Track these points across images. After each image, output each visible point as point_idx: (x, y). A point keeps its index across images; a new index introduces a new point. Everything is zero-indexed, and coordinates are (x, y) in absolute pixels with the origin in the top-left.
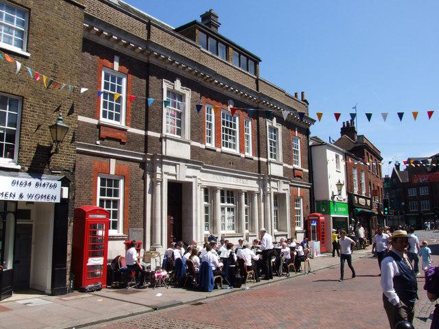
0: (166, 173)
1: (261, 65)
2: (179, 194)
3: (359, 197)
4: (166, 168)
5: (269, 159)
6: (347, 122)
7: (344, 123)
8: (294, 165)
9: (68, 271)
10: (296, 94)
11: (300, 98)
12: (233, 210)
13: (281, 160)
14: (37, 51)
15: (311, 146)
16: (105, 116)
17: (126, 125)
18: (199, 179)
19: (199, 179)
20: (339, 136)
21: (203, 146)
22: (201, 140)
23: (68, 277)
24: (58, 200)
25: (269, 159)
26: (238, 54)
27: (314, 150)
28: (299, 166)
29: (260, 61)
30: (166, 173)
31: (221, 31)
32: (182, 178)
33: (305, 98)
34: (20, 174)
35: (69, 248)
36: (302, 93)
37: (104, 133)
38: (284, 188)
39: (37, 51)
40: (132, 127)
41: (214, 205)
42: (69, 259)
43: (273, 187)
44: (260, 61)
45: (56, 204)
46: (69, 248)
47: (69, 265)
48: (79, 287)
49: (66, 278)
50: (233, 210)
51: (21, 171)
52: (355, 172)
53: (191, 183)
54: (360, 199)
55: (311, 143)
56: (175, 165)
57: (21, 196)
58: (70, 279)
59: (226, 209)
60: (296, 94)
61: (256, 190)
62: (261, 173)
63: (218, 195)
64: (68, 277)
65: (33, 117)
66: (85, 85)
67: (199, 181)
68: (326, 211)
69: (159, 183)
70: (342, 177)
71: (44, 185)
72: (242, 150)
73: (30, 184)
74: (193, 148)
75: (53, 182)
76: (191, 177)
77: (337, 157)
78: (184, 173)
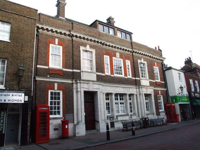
0: (83, 87)
1: (133, 35)
2: (90, 97)
3: (194, 93)
4: (82, 85)
5: (141, 78)
6: (187, 58)
7: (186, 59)
8: (156, 80)
9: (29, 133)
10: (156, 48)
11: (157, 49)
12: (123, 103)
13: (148, 78)
14: (14, 39)
15: (165, 71)
16: (115, 74)
17: (63, 68)
18: (102, 89)
19: (102, 89)
20: (184, 65)
21: (104, 75)
22: (154, 79)
23: (28, 137)
24: (23, 102)
25: (141, 78)
26: (120, 32)
27: (166, 72)
28: (159, 81)
29: (132, 34)
30: (83, 87)
31: (116, 25)
32: (91, 89)
33: (160, 49)
34: (5, 91)
35: (29, 124)
36: (159, 47)
37: (50, 72)
38: (150, 91)
39: (14, 39)
40: (65, 68)
41: (112, 101)
42: (29, 128)
43: (144, 91)
44: (132, 34)
45: (23, 103)
46: (29, 124)
47: (29, 131)
48: (34, 141)
49: (27, 137)
50: (123, 103)
51: (6, 90)
52: (191, 81)
53: (97, 92)
54: (196, 94)
55: (164, 69)
56: (88, 83)
57: (5, 101)
58: (29, 138)
59: (119, 103)
60: (156, 48)
61: (135, 93)
62: (137, 83)
63: (128, 97)
64: (28, 137)
65: (11, 66)
66: (79, 58)
67: (101, 91)
68: (175, 101)
69: (80, 92)
70: (184, 84)
71: (16, 95)
72: (126, 75)
73: (9, 95)
74: (97, 76)
75: (20, 94)
76: (96, 89)
77: (179, 74)
78: (92, 87)
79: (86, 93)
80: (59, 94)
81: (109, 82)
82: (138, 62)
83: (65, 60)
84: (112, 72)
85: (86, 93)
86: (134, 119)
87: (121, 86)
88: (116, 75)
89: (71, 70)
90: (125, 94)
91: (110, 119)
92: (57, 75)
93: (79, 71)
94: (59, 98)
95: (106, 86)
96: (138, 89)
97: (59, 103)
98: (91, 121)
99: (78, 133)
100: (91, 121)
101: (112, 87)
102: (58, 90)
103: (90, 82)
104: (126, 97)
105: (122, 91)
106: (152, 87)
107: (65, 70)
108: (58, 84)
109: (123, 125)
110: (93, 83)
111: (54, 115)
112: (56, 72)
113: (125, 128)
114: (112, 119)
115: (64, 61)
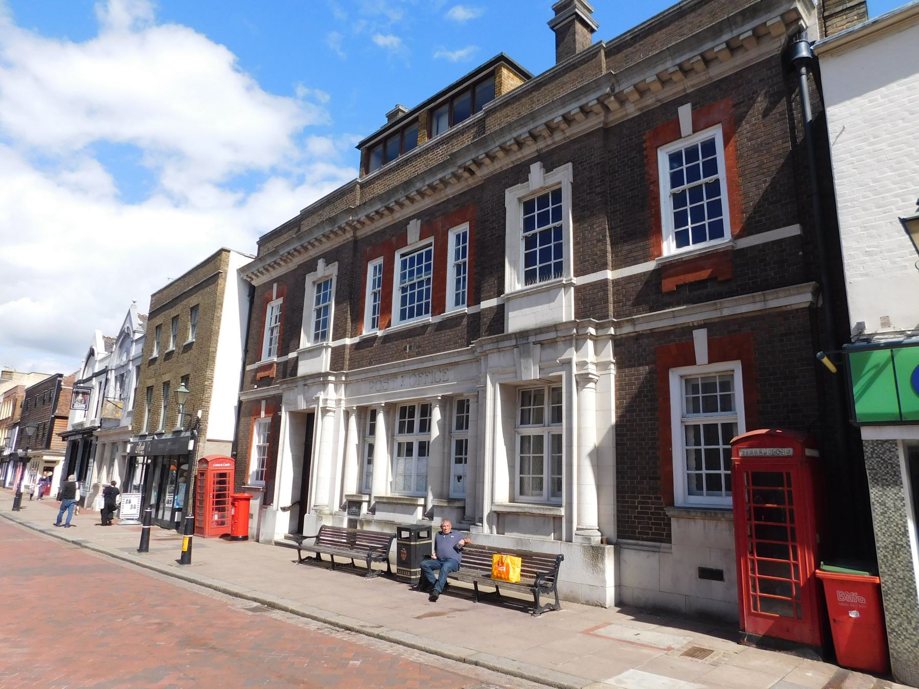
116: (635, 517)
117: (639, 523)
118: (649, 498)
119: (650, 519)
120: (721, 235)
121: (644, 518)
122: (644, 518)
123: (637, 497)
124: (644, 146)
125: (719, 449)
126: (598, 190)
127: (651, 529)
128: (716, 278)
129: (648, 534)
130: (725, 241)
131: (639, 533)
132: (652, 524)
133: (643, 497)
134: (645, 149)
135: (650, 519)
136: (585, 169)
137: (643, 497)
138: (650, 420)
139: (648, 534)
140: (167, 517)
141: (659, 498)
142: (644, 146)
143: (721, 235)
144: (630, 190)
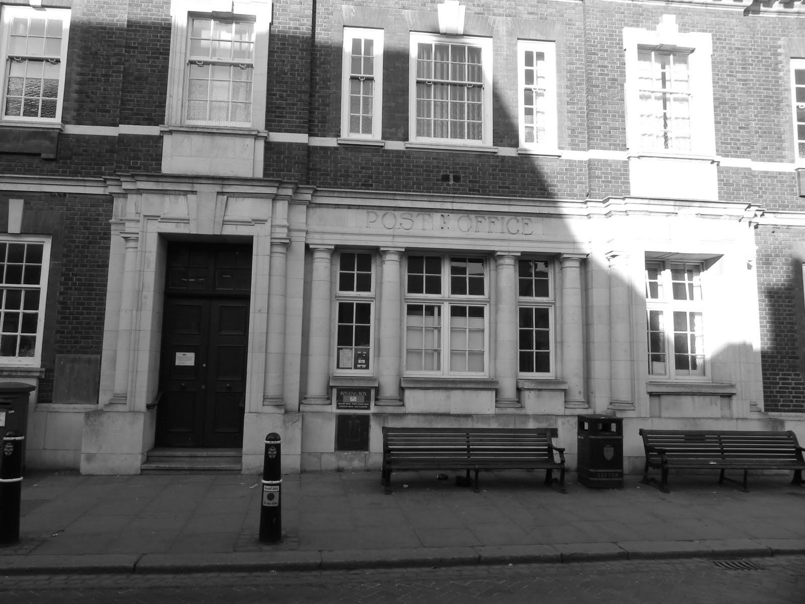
21: (330, 142)
40: (79, 123)
59: (446, 310)
79: (178, 250)
80: (35, 253)
81: (367, 186)
82: (620, 43)
83: (78, 78)
84: (396, 122)
85: (178, 250)
86: (537, 417)
87: (456, 206)
88: (415, 140)
89: (301, 138)
90: (485, 257)
91: (340, 398)
92: (26, 160)
93: (278, 137)
94: (34, 276)
95: (337, 206)
96: (282, 206)
97: (32, 300)
98: (198, 403)
99: (90, 458)
100: (198, 403)
101: (380, 213)
102: (24, 232)
103: (197, 187)
104: (497, 275)
105: (459, 234)
106: (738, 209)
107: (73, 129)
108: (26, 203)
109: (648, 449)
110: (218, 188)
111: (469, 372)
112: (19, 146)
113: (656, 466)
114: (353, 399)
115: (75, 87)
116: (777, 392)
117: (781, 397)
118: (790, 375)
119: (791, 393)
120: (52, 114)
121: (785, 392)
122: (785, 392)
123: (778, 375)
124: (779, 51)
125: (19, 309)
126: (739, 76)
127: (792, 401)
128: (39, 155)
129: (789, 406)
130: (56, 120)
131: (782, 406)
132: (794, 397)
133: (783, 375)
134: (780, 54)
135: (791, 393)
136: (724, 47)
137: (783, 375)
138: (788, 306)
139: (789, 406)
140: (270, 453)
141: (798, 375)
142: (779, 51)
143: (52, 114)
144: (765, 89)
